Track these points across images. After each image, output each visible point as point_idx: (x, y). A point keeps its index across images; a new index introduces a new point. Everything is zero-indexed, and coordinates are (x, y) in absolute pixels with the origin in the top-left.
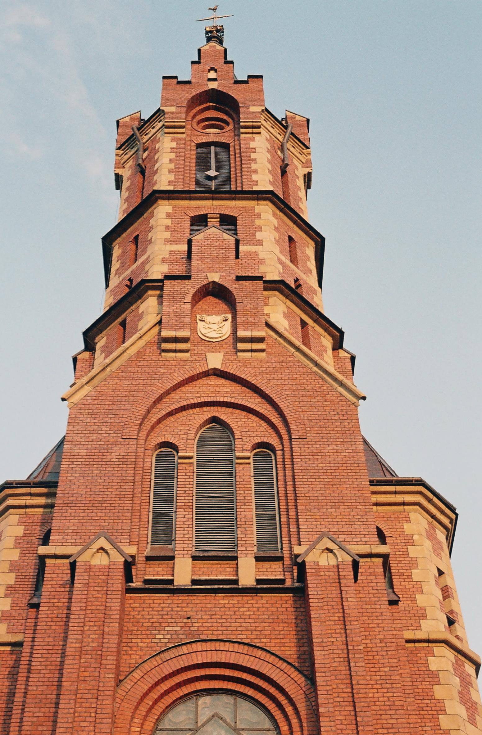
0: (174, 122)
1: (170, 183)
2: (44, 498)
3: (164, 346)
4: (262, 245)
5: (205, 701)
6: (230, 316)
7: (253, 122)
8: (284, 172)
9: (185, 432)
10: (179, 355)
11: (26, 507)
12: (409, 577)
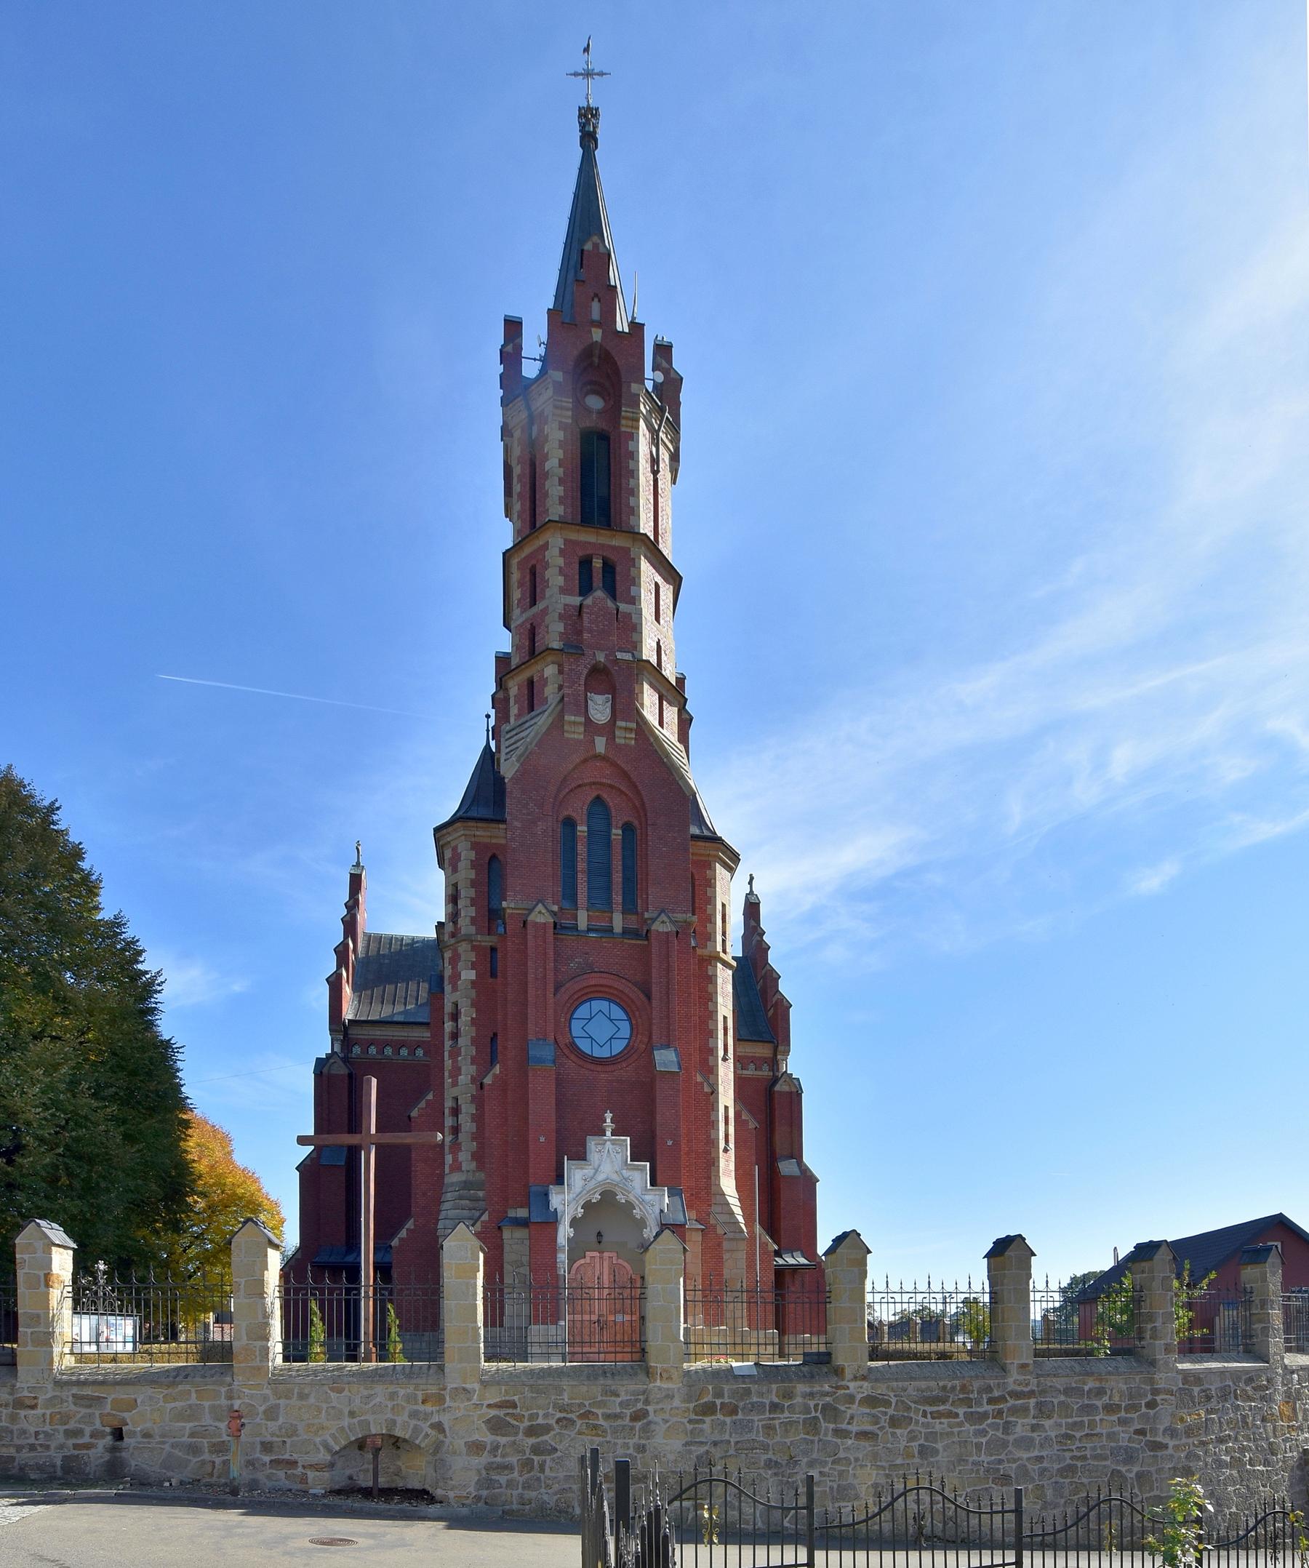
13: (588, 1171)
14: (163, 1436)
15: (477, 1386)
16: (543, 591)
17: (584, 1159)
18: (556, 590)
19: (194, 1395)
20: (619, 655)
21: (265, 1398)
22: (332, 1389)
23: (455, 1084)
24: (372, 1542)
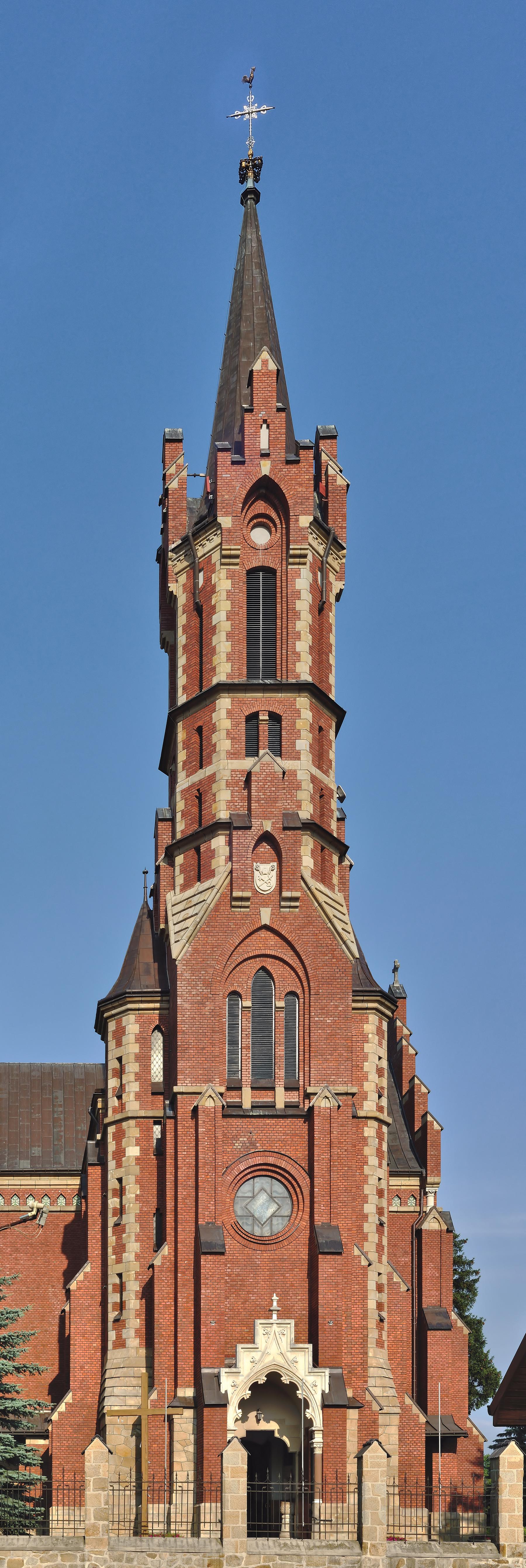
0: (230, 549)
1: (228, 675)
2: (434, 1455)
4: (299, 759)
5: (256, 1179)
6: (275, 864)
7: (301, 549)
8: (321, 610)
9: (244, 982)
10: (242, 910)
12: (362, 1068)
13: (257, 1355)
15: (244, 1555)
16: (210, 757)
18: (223, 755)
19: (59, 1558)
20: (201, 575)
21: (105, 1561)
22: (149, 1556)
23: (119, 1261)
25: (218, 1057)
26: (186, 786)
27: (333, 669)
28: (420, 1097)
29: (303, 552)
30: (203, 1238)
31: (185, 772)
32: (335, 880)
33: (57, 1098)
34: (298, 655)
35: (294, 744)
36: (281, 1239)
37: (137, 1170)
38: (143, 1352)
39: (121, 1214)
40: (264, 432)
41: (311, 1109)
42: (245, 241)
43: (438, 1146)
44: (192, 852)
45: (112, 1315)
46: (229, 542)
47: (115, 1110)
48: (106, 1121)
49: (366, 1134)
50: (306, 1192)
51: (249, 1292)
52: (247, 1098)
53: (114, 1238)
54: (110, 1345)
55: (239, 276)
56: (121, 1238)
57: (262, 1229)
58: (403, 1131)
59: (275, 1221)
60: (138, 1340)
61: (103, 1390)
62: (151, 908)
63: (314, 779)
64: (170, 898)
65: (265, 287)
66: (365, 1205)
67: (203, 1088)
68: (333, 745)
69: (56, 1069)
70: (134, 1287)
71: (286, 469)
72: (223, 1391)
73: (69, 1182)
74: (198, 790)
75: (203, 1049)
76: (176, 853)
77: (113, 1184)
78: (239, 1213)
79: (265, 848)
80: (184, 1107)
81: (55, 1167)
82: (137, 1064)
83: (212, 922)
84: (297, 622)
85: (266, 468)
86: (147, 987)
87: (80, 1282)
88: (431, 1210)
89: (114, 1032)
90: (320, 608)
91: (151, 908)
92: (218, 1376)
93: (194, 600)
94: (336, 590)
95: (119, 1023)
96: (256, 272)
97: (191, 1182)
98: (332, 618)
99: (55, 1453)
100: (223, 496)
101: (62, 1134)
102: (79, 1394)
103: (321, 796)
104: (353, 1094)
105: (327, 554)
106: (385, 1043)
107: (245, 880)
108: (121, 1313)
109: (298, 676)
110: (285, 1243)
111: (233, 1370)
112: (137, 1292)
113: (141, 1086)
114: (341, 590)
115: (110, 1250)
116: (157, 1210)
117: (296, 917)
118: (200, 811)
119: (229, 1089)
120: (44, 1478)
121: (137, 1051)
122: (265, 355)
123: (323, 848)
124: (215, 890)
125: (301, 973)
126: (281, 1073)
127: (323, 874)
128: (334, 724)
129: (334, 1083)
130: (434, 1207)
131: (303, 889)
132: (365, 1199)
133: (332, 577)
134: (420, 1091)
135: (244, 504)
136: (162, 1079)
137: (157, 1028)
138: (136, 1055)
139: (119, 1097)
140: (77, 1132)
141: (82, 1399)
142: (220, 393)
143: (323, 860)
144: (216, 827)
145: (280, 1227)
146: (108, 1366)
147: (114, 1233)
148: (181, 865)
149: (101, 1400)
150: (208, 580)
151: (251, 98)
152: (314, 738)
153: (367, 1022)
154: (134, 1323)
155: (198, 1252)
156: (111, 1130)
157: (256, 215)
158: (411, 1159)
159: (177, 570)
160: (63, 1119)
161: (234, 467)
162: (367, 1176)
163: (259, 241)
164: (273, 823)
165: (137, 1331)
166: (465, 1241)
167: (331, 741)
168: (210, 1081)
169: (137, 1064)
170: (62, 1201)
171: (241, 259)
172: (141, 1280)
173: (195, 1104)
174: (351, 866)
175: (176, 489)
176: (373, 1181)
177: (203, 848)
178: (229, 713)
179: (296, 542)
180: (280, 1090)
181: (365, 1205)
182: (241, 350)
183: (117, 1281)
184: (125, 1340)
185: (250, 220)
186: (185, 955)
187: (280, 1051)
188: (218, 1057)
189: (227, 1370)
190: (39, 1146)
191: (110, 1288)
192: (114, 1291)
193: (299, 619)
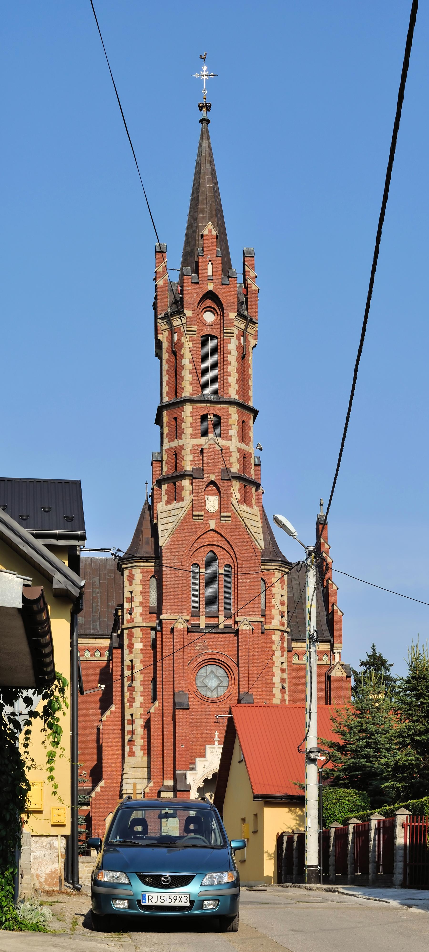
1: (191, 394)
3: (194, 517)
4: (231, 440)
6: (218, 497)
8: (243, 357)
9: (201, 558)
11: (142, 566)
12: (271, 602)
13: (207, 764)
14: (85, 878)
16: (181, 435)
17: (204, 756)
18: (188, 436)
20: (176, 335)
23: (131, 707)
24: (289, 800)
25: (186, 599)
26: (168, 447)
27: (251, 387)
28: (332, 592)
29: (231, 331)
30: (177, 700)
31: (167, 439)
32: (253, 501)
33: (95, 582)
34: (230, 385)
35: (228, 432)
36: (222, 700)
37: (141, 656)
38: (146, 758)
39: (132, 680)
40: (210, 267)
41: (238, 630)
42: (201, 146)
43: (340, 625)
44: (172, 485)
45: (127, 737)
46: (190, 324)
47: (128, 621)
48: (123, 627)
49: (274, 639)
50: (236, 674)
51: (204, 728)
52: (203, 622)
53: (128, 693)
54: (126, 755)
55: (199, 165)
56: (132, 694)
57: (212, 693)
58: (323, 611)
59: (219, 689)
60: (142, 752)
61: (122, 780)
62: (150, 504)
63: (239, 450)
64: (161, 507)
65: (213, 173)
66: (274, 678)
67: (177, 617)
68: (252, 428)
69: (94, 561)
70: (140, 722)
71: (222, 287)
72: (188, 783)
73: (103, 642)
74: (175, 451)
75: (178, 595)
76: (162, 483)
77: (127, 663)
78: (199, 684)
79: (212, 488)
80: (166, 627)
81: (93, 632)
82: (141, 596)
83: (183, 526)
84: (229, 367)
85: (210, 286)
86: (147, 553)
87: (108, 716)
88: (337, 664)
89: (128, 577)
90: (243, 357)
91: (150, 504)
92: (185, 775)
93: (172, 349)
94: (252, 345)
95: (130, 572)
96: (208, 166)
97: (171, 668)
98: (250, 360)
99: (93, 815)
100: (187, 299)
101: (99, 607)
102: (108, 781)
103: (244, 458)
104: (262, 622)
105: (246, 327)
106: (285, 587)
107: (200, 506)
108: (132, 737)
109: (230, 396)
110: (225, 702)
111: (193, 771)
112: (141, 725)
113: (143, 609)
114: (256, 345)
115: (126, 700)
116: (153, 679)
117: (229, 525)
118: (176, 463)
119: (192, 616)
120: (87, 831)
121: (141, 589)
122: (210, 225)
123: (245, 486)
124: (184, 510)
125: (233, 555)
126: (222, 608)
127: (246, 500)
128: (252, 417)
129: (251, 616)
130: (338, 662)
131: (232, 510)
132: (273, 674)
133: (250, 338)
134: (332, 588)
135: (198, 304)
136: (156, 605)
137: (153, 576)
138: (141, 591)
139: (131, 614)
140: (109, 606)
141: (110, 784)
142: (187, 229)
143: (246, 492)
144: (183, 476)
145: (222, 693)
146: (125, 766)
147: (128, 691)
148: (165, 490)
149: (121, 786)
150: (179, 339)
151: (205, 68)
152: (239, 428)
153: (274, 577)
154: (140, 742)
155: (174, 709)
156: (126, 632)
157: (208, 132)
158: (325, 631)
159: (162, 328)
160: (99, 597)
161: (193, 285)
162: (274, 662)
163: (210, 147)
164: (216, 476)
165: (142, 747)
166: (392, 665)
167: (250, 427)
168: (181, 613)
169: (141, 596)
170: (98, 654)
171: (199, 156)
172: (144, 718)
173: (172, 626)
174: (263, 493)
175: (162, 286)
176: (278, 664)
177: (177, 484)
178: (191, 413)
179: (228, 326)
180: (221, 618)
181: (274, 678)
182: (199, 210)
183: (130, 718)
184: (135, 752)
185: (205, 135)
186: (167, 544)
187: (222, 597)
188: (186, 599)
189: (190, 772)
190: (82, 617)
191: (126, 722)
192: (128, 724)
193: (230, 365)
